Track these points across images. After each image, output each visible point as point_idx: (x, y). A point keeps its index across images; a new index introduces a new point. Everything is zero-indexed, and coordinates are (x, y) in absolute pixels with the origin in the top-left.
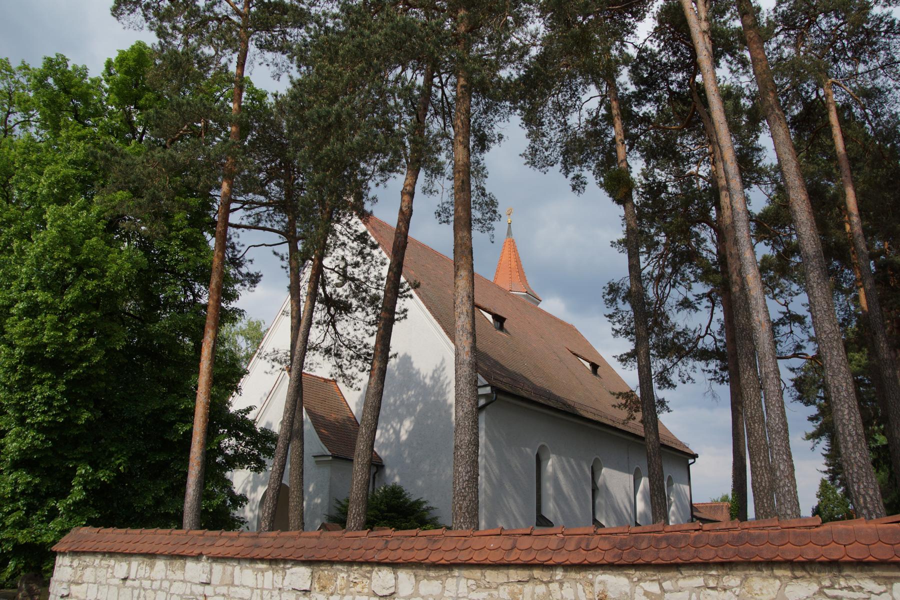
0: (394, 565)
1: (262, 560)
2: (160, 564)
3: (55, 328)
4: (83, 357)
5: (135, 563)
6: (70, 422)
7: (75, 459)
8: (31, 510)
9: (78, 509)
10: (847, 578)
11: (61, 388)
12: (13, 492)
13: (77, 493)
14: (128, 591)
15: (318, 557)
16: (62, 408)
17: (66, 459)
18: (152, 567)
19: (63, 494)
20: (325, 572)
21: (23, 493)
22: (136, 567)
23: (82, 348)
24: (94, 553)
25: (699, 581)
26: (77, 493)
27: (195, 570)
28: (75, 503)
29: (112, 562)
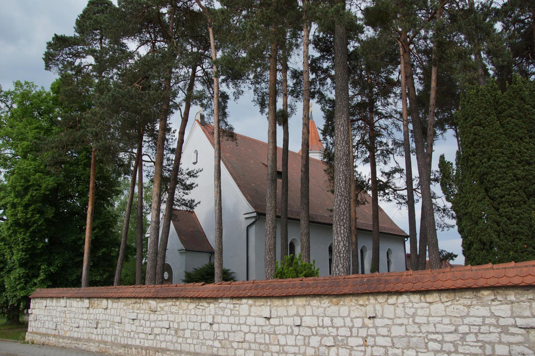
0: (107, 298)
1: (78, 298)
2: (55, 300)
3: (22, 212)
4: (35, 222)
5: (48, 300)
6: (34, 248)
7: (41, 262)
8: (26, 283)
9: (43, 282)
10: (202, 302)
11: (28, 234)
12: (19, 276)
13: (42, 276)
14: (46, 311)
15: (92, 295)
16: (29, 242)
17: (38, 262)
18: (52, 302)
19: (37, 276)
20: (92, 301)
21: (22, 276)
22: (49, 302)
23: (33, 219)
24: (38, 298)
25: (171, 303)
26: (42, 276)
27: (63, 302)
28: (41, 280)
29: (43, 301)
